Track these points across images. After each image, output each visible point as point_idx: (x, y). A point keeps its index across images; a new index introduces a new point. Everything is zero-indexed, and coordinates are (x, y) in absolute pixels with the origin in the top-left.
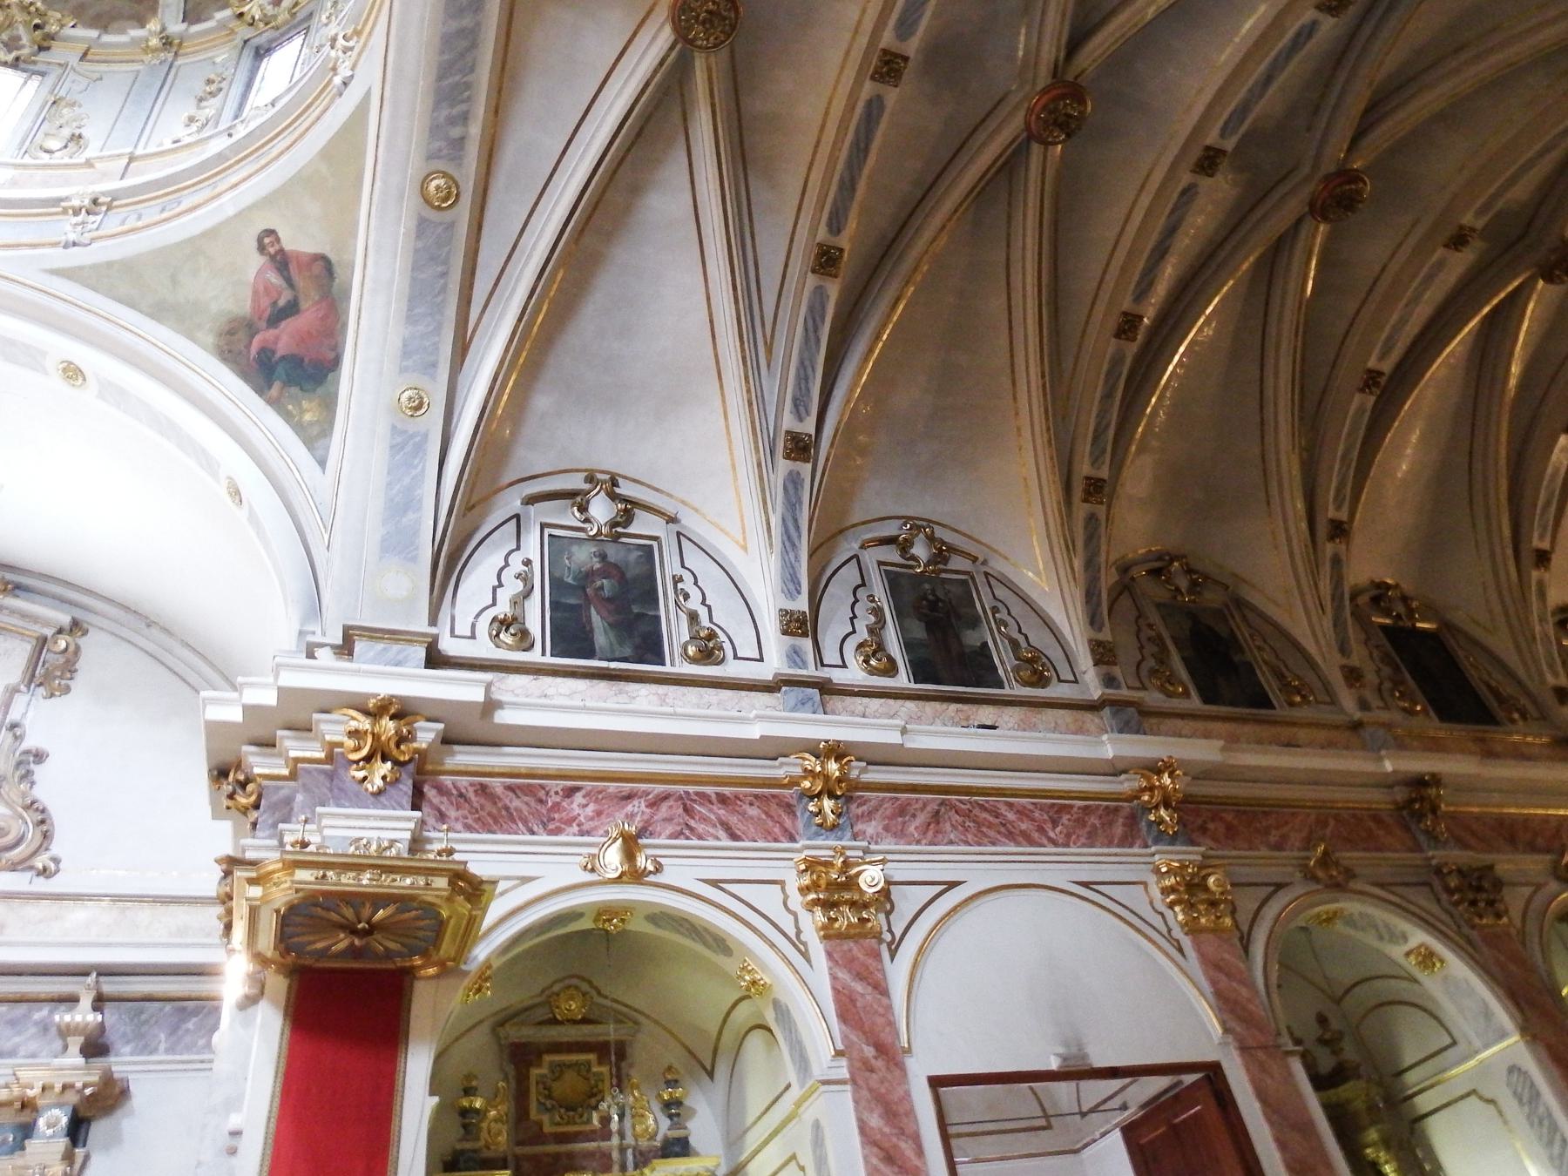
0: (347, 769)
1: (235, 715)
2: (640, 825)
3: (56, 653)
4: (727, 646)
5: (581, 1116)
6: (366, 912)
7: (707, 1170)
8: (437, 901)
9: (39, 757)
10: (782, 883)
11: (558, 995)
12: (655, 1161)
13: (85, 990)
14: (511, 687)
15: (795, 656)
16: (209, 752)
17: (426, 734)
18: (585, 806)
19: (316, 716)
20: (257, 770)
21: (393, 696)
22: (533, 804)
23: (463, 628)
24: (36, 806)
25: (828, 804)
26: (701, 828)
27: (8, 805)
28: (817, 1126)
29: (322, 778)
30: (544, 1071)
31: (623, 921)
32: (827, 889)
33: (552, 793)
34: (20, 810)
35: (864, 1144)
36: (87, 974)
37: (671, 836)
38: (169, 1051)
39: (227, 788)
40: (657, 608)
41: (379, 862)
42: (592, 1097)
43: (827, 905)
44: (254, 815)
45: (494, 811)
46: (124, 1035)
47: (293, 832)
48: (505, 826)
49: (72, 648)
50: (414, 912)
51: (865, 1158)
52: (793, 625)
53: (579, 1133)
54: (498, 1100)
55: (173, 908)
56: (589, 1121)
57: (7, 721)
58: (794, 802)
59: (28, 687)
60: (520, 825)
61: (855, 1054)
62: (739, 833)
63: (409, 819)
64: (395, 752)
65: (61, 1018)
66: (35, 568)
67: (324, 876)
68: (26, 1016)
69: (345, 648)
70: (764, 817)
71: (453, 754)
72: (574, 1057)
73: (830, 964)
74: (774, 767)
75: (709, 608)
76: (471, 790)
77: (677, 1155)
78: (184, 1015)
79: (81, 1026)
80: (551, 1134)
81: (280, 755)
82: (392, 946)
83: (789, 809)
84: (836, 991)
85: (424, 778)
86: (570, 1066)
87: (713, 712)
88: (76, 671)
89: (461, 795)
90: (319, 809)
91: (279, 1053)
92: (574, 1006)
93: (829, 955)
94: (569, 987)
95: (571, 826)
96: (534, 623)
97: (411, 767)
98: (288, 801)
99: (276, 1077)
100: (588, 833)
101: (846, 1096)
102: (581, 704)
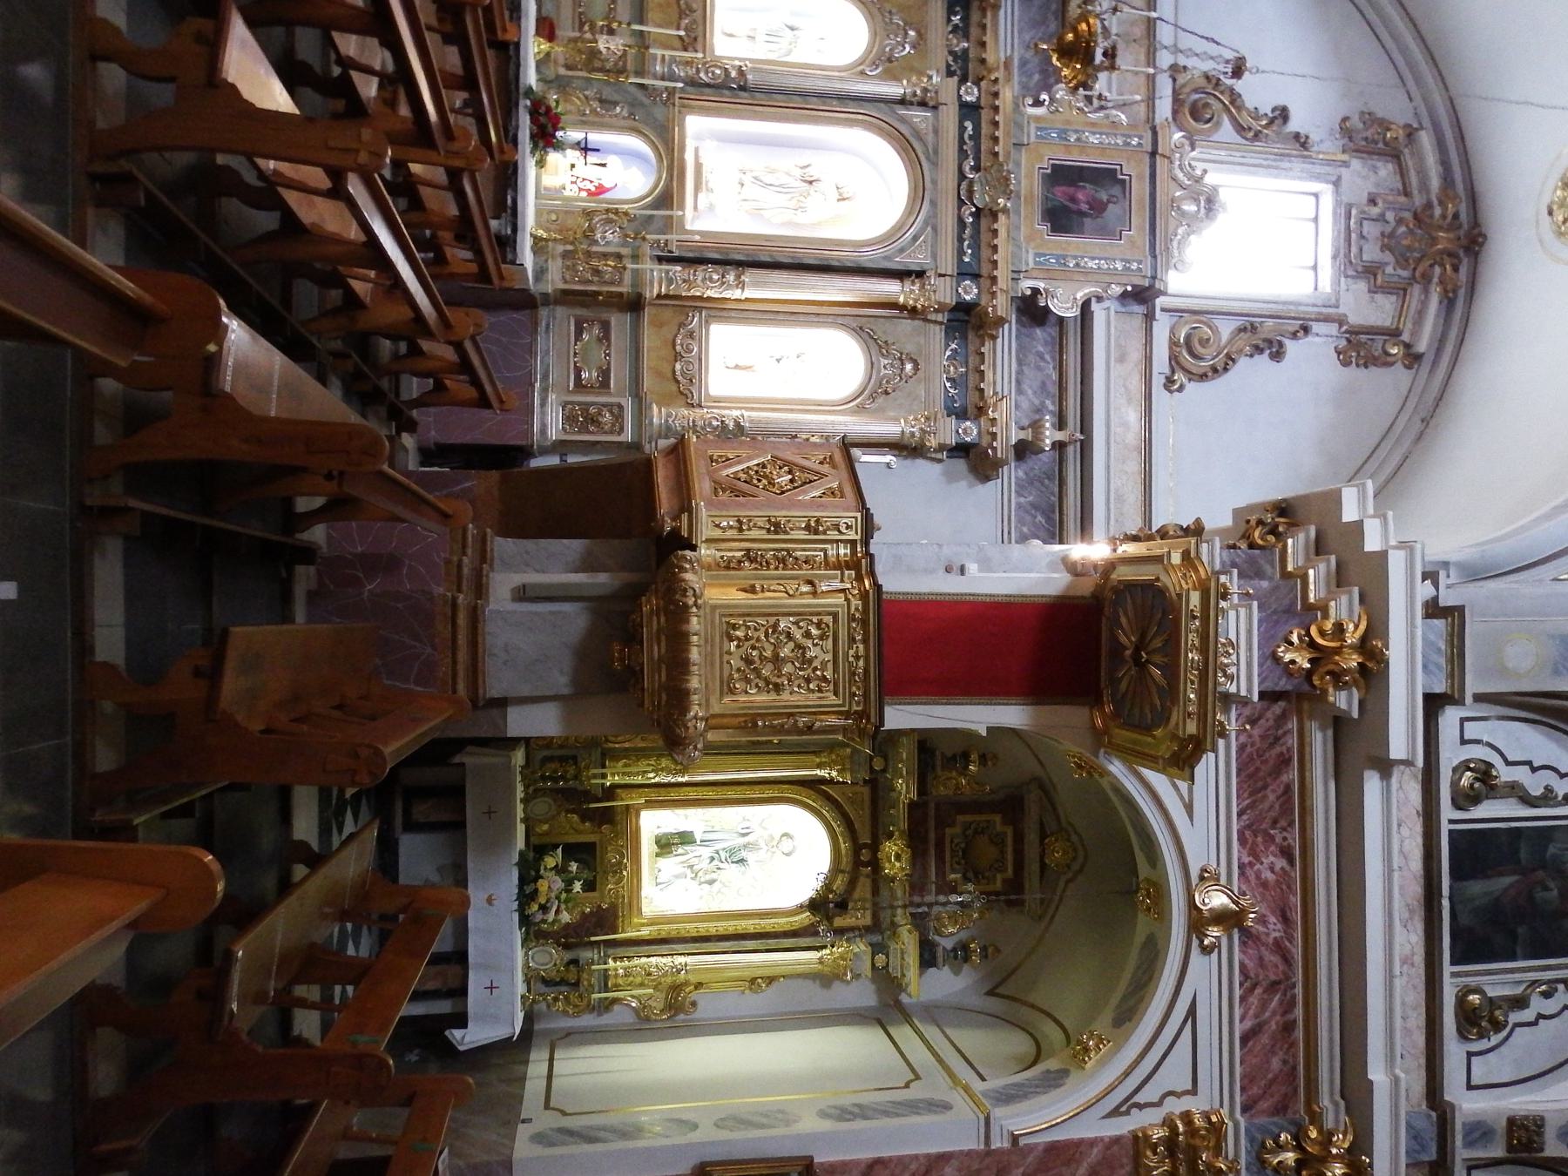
0: (1300, 626)
2: (1254, 931)
4: (1483, 1045)
5: (958, 863)
6: (1157, 659)
7: (907, 985)
9: (1278, 355)
10: (1194, 1091)
11: (1069, 840)
12: (916, 934)
13: (1073, 430)
14: (1409, 790)
15: (1479, 1132)
16: (1306, 497)
17: (1345, 700)
18: (1272, 870)
19: (1356, 590)
20: (1290, 541)
22: (1273, 814)
23: (1472, 730)
24: (1230, 363)
25: (1290, 1157)
26: (1254, 1000)
27: (1229, 342)
28: (946, 1107)
29: (1286, 602)
30: (999, 828)
31: (1149, 909)
32: (1189, 1145)
33: (1285, 834)
34: (1225, 352)
35: (928, 1156)
37: (1243, 966)
38: (1019, 506)
39: (1269, 518)
40: (1526, 958)
42: (974, 873)
43: (1171, 1142)
44: (1244, 546)
45: (1261, 774)
46: (1032, 469)
47: (1232, 582)
48: (1245, 786)
49: (1389, 359)
50: (1158, 703)
51: (916, 1157)
52: (1523, 1133)
53: (944, 863)
54: (975, 786)
56: (954, 871)
57: (1311, 323)
58: (1290, 1114)
59: (1346, 332)
60: (1247, 802)
61: (1014, 1158)
62: (1250, 1044)
63: (1249, 690)
65: (1047, 421)
67: (1194, 617)
68: (1048, 395)
69: (1433, 610)
70: (1270, 1076)
71: (1323, 729)
72: (1010, 857)
73: (1107, 1140)
74: (1332, 1094)
75: (1534, 1023)
77: (921, 956)
79: (1042, 437)
80: (944, 834)
82: (1123, 686)
83: (1281, 1109)
84: (1081, 1142)
85: (1294, 701)
86: (1002, 852)
87: (1398, 1023)
88: (1366, 367)
89: (1277, 739)
90: (1255, 604)
91: (1026, 596)
92: (1057, 855)
93: (1117, 1140)
94: (1075, 850)
95: (1249, 855)
96: (1489, 810)
97: (1306, 687)
98: (1259, 574)
100: (1242, 874)
101: (973, 1143)
102: (1395, 866)
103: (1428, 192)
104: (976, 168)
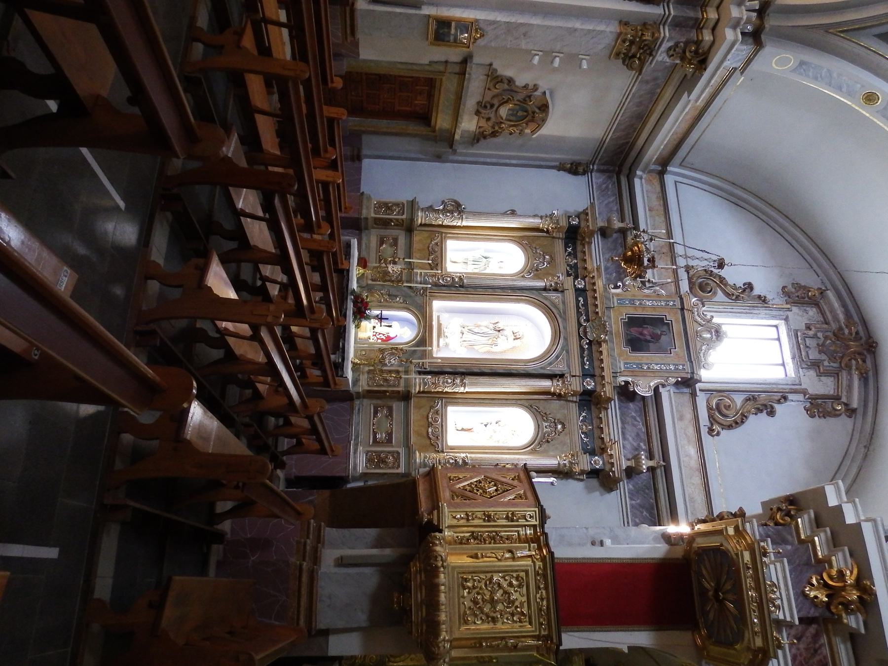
1: (832, 502)
3: (832, 406)
6: (730, 596)
8: (746, 639)
17: (854, 621)
21: (876, 595)
36: (664, 461)
38: (632, 506)
41: (764, 601)
44: (772, 524)
46: (637, 484)
47: (769, 546)
49: (838, 413)
50: (735, 626)
55: (703, 493)
59: (809, 398)
63: (792, 616)
64: (836, 602)
66: (880, 380)
67: (748, 568)
71: (844, 642)
76: (821, 657)
78: (650, 510)
81: (812, 531)
82: (711, 615)
88: (825, 418)
89: (816, 651)
90: (785, 560)
97: (828, 614)
98: (785, 542)
99: (630, 559)
103: (839, 321)
104: (587, 320)
